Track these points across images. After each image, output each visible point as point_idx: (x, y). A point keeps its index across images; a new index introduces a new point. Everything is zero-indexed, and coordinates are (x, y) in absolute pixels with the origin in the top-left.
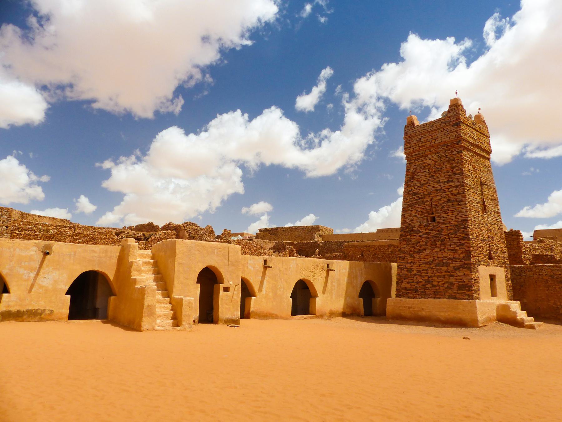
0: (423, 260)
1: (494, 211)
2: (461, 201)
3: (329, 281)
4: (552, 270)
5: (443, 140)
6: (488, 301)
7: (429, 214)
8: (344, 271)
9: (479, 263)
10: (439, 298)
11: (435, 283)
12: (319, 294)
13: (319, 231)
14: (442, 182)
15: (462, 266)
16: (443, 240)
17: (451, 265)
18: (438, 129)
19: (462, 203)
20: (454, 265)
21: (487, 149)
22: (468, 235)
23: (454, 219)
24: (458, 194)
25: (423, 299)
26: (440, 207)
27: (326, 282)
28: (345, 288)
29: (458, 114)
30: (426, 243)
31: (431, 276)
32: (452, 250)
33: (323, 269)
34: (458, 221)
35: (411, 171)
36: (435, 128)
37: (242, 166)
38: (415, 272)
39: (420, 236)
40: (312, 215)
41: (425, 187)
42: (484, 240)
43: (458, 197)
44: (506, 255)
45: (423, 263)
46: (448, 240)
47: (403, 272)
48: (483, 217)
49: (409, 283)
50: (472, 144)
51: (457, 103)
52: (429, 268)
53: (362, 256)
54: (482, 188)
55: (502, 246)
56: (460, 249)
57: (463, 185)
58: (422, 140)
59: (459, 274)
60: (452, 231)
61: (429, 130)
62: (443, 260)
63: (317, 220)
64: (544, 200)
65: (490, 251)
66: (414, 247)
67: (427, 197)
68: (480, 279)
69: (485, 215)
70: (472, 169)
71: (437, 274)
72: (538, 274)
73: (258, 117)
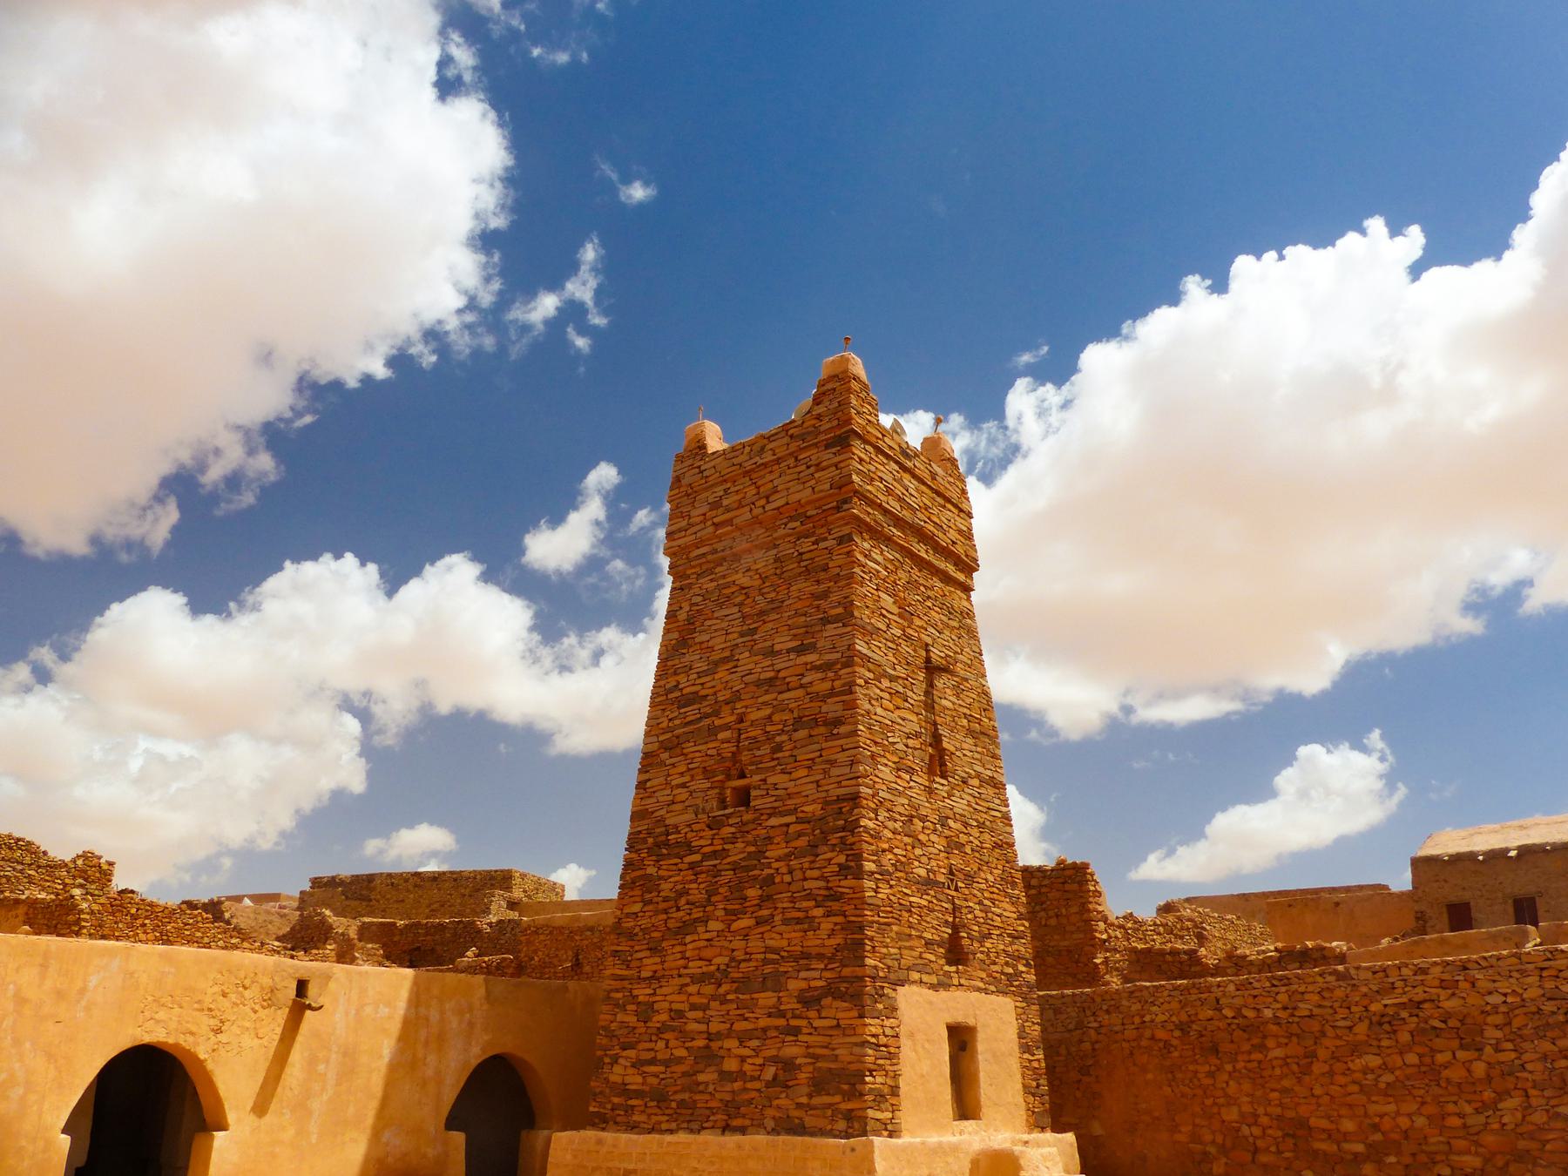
0: (695, 967)
1: (978, 775)
2: (838, 722)
3: (297, 1056)
4: (1183, 1005)
5: (794, 498)
6: (933, 1139)
7: (729, 778)
8: (384, 1011)
9: (902, 975)
10: (743, 1130)
11: (731, 1065)
12: (231, 1117)
13: (508, 888)
14: (780, 652)
15: (831, 991)
16: (769, 881)
17: (794, 985)
18: (778, 461)
19: (843, 729)
20: (803, 985)
21: (959, 549)
22: (858, 857)
23: (810, 789)
24: (833, 693)
25: (682, 1137)
26: (765, 750)
27: (280, 1059)
28: (377, 1083)
29: (844, 404)
30: (710, 894)
31: (719, 1036)
32: (799, 921)
33: (269, 999)
34: (826, 803)
35: (682, 616)
36: (768, 457)
37: (360, 708)
38: (664, 1017)
39: (692, 866)
40: (573, 867)
41: (722, 674)
42: (929, 883)
43: (832, 708)
44: (1023, 948)
45: (695, 979)
46: (787, 878)
47: (620, 1017)
48: (930, 791)
49: (638, 1064)
50: (898, 522)
51: (846, 371)
52: (713, 998)
53: (577, 964)
54: (931, 685)
55: (1007, 911)
56: (828, 915)
57: (850, 659)
58: (725, 502)
59: (817, 1023)
60: (802, 842)
61: (748, 465)
62: (766, 962)
63: (590, 880)
64: (1194, 833)
65: (956, 928)
66: (666, 911)
67: (726, 710)
68: (905, 1042)
69: (941, 786)
70: (895, 610)
71: (741, 1026)
72: (1137, 1020)
73: (429, 570)
